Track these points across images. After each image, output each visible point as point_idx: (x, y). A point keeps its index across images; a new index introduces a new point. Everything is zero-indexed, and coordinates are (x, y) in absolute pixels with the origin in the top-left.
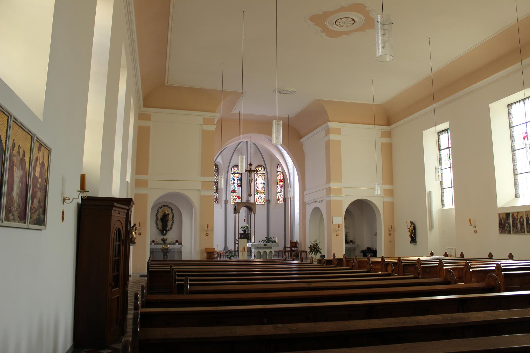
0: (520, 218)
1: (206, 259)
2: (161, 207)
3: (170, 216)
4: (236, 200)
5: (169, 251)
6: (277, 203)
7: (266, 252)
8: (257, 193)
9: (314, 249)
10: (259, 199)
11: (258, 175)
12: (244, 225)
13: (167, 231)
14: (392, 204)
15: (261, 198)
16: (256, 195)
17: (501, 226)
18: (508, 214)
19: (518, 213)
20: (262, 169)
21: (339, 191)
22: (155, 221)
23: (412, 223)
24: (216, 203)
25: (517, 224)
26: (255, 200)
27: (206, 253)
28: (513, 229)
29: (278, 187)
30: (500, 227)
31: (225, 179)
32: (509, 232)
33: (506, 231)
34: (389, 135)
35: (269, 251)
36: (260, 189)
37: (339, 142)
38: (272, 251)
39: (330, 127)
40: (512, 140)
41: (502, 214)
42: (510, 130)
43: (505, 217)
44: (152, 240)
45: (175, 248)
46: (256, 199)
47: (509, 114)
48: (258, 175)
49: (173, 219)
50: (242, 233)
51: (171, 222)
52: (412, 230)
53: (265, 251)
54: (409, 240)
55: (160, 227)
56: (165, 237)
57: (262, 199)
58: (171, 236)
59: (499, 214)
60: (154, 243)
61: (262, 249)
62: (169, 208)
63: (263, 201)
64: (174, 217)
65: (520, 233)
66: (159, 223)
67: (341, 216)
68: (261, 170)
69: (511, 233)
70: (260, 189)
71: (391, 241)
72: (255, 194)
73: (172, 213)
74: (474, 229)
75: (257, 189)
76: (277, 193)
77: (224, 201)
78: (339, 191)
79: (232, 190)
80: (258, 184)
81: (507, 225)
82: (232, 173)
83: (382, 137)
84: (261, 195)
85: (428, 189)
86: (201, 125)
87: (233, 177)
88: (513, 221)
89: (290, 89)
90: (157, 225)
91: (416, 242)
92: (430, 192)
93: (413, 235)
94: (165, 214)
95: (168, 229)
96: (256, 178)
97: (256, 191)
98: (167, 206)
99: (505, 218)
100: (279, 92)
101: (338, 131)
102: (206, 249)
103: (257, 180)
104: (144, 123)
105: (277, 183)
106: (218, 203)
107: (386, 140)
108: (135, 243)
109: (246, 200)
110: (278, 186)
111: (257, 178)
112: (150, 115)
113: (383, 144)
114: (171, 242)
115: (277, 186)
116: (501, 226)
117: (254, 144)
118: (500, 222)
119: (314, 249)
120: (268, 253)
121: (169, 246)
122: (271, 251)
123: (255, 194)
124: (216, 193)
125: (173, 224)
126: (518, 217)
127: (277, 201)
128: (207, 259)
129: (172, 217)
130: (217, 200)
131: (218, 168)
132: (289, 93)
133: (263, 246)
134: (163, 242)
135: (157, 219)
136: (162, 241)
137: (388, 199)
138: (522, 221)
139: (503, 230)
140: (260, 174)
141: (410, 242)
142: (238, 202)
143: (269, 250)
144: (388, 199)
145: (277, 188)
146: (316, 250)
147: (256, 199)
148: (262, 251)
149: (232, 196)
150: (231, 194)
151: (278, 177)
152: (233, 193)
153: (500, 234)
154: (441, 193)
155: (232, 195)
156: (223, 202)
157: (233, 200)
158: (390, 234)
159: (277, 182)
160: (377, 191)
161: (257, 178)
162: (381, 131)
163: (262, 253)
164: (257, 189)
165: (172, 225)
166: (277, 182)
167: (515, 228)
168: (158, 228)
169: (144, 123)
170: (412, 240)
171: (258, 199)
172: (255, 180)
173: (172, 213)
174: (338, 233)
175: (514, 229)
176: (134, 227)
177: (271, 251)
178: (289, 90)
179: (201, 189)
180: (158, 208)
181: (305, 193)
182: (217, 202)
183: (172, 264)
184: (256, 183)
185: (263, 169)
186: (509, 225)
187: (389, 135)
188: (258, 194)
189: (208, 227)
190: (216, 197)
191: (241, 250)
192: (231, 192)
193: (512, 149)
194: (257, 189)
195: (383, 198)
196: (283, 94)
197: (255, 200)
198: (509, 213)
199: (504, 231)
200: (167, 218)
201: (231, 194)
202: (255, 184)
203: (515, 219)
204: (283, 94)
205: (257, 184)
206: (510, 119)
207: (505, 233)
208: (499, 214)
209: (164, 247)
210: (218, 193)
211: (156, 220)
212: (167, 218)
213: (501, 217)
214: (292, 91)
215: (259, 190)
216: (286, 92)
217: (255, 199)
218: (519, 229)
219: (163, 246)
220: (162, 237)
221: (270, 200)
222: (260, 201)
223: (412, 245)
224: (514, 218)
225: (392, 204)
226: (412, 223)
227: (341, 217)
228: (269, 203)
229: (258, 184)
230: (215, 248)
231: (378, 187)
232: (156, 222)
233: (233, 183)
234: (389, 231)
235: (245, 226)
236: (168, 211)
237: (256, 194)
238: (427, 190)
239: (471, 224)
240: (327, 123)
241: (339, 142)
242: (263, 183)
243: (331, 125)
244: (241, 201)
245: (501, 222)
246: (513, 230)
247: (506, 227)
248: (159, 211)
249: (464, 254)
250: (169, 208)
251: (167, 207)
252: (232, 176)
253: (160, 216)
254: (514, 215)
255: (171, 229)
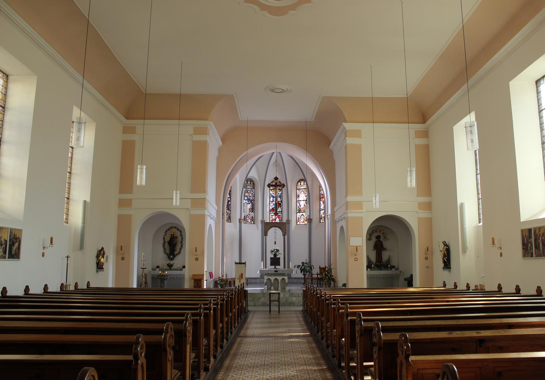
0: (542, 236)
1: (193, 288)
2: (169, 229)
3: (179, 239)
4: (275, 220)
5: (165, 277)
6: (320, 222)
7: (278, 280)
8: (300, 211)
9: (325, 277)
10: (302, 218)
11: (301, 191)
12: (274, 248)
13: (174, 256)
14: (430, 219)
15: (304, 217)
16: (298, 214)
17: (524, 247)
18: (530, 230)
19: (540, 228)
20: (304, 184)
21: (359, 205)
22: (162, 245)
23: (445, 244)
24: (251, 224)
25: (539, 244)
26: (298, 220)
27: (193, 280)
28: (535, 251)
29: (321, 204)
30: (523, 249)
31: (262, 197)
32: (532, 256)
33: (528, 253)
34: (425, 134)
35: (274, 279)
36: (302, 206)
37: (359, 147)
38: (285, 278)
39: (347, 129)
40: (542, 129)
41: (525, 230)
42: (539, 115)
43: (527, 234)
44: (157, 266)
45: (181, 274)
46: (299, 218)
47: (538, 93)
48: (301, 191)
49: (181, 242)
50: (273, 258)
51: (180, 246)
52: (444, 254)
53: (276, 279)
54: (442, 265)
55: (168, 251)
56: (172, 262)
57: (305, 218)
58: (177, 262)
59: (522, 231)
60: (158, 269)
61: (273, 276)
62: (178, 230)
63: (306, 221)
64: (183, 239)
65: (543, 257)
66: (167, 246)
67: (361, 236)
68: (303, 184)
69: (533, 257)
70: (302, 206)
71: (427, 267)
72: (297, 212)
73: (181, 235)
74: (500, 251)
75: (299, 207)
76: (320, 211)
77: (261, 221)
78: (359, 205)
79: (271, 208)
80: (301, 201)
81: (529, 245)
82: (271, 189)
83: (416, 137)
84: (304, 214)
85: (460, 200)
86: (191, 135)
87: (272, 194)
88: (535, 240)
89: (284, 87)
90: (165, 249)
91: (450, 268)
92: (461, 203)
93: (446, 259)
94: (172, 237)
95: (176, 253)
96: (298, 194)
97: (298, 209)
98: (175, 227)
99: (528, 236)
100: (272, 90)
101: (357, 134)
102: (194, 275)
103: (299, 197)
104: (129, 137)
105: (320, 199)
106: (254, 223)
107: (421, 141)
108: (103, 268)
109: (286, 219)
110: (321, 202)
111: (299, 195)
112: (135, 127)
113: (417, 146)
114: (178, 268)
115: (320, 203)
116: (524, 247)
117: (289, 157)
118: (523, 241)
119: (325, 277)
120: (280, 281)
121: (166, 272)
122: (283, 279)
123: (297, 212)
124: (251, 212)
125: (182, 247)
126: (540, 234)
127: (320, 220)
128: (195, 287)
129: (181, 240)
130: (253, 221)
131: (254, 184)
132: (283, 91)
133: (274, 273)
134: (169, 268)
135: (165, 242)
136: (168, 267)
137: (424, 214)
138: (544, 240)
139: (526, 252)
140: (303, 190)
141: (443, 268)
142: (278, 222)
143: (281, 278)
144: (424, 214)
145: (320, 204)
146: (327, 278)
147: (299, 218)
148: (272, 278)
149: (270, 216)
150: (270, 213)
151: (321, 192)
152: (272, 212)
153: (524, 258)
154: (478, 204)
155: (271, 214)
156: (238, 221)
157: (273, 220)
158: (426, 258)
159: (320, 198)
160: (376, 204)
161: (299, 195)
162: (194, 127)
163: (272, 281)
164: (300, 206)
165: (180, 249)
166: (320, 198)
167: (537, 250)
168: (165, 252)
169: (129, 137)
170: (445, 266)
171: (300, 218)
172: (298, 196)
173: (181, 235)
174: (356, 257)
175: (536, 250)
176: (102, 251)
177: (283, 279)
178: (281, 88)
179: (190, 207)
180: (166, 230)
181: (335, 209)
182: (252, 223)
183: (225, 292)
184: (298, 200)
185: (305, 183)
186: (532, 245)
187: (425, 134)
188: (300, 212)
189: (196, 251)
190: (252, 217)
191: (238, 277)
192: (270, 211)
193: (541, 140)
194: (299, 207)
195: (417, 213)
196: (278, 93)
197: (298, 220)
198: (531, 229)
199: (526, 253)
200: (174, 241)
201: (270, 213)
202: (297, 201)
203: (538, 237)
204: (278, 93)
205: (299, 201)
206: (539, 100)
207: (528, 256)
208: (522, 231)
209: (161, 274)
210: (254, 213)
211: (163, 243)
212: (174, 241)
213: (524, 234)
214: (287, 89)
215: (301, 207)
216: (280, 91)
217: (297, 218)
218: (541, 251)
219: (160, 272)
220: (169, 262)
221: (311, 219)
222: (302, 221)
223: (446, 272)
224: (536, 236)
225: (430, 219)
226: (445, 244)
227: (361, 238)
228: (311, 222)
229: (301, 201)
230: (193, 275)
231: (376, 199)
232: (164, 245)
233: (272, 200)
234: (426, 254)
235: (275, 250)
236: (178, 234)
237: (298, 212)
238: (459, 201)
239: (493, 245)
240: (342, 124)
241: (359, 147)
242: (305, 199)
243: (348, 126)
244: (282, 221)
245: (524, 242)
246: (535, 253)
247: (529, 249)
248: (166, 234)
249: (90, 283)
250: (178, 230)
251: (175, 229)
252: (271, 192)
253: (168, 239)
254: (536, 232)
255: (180, 253)
